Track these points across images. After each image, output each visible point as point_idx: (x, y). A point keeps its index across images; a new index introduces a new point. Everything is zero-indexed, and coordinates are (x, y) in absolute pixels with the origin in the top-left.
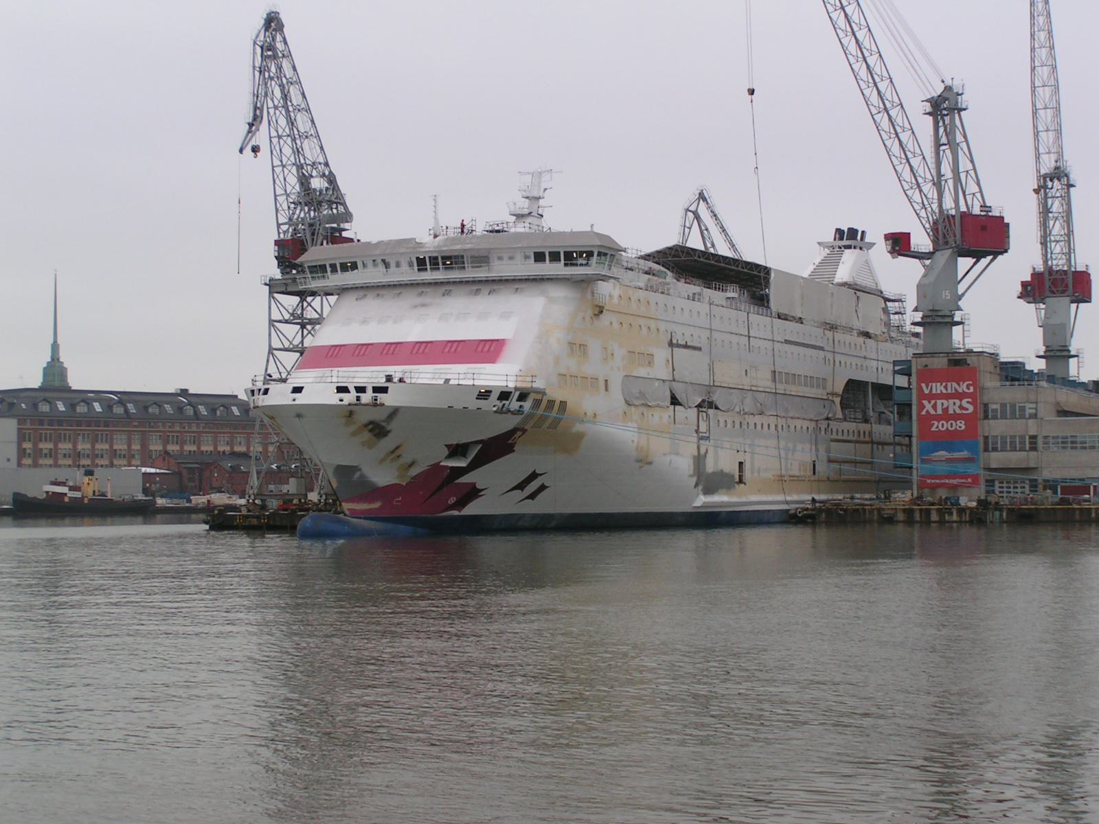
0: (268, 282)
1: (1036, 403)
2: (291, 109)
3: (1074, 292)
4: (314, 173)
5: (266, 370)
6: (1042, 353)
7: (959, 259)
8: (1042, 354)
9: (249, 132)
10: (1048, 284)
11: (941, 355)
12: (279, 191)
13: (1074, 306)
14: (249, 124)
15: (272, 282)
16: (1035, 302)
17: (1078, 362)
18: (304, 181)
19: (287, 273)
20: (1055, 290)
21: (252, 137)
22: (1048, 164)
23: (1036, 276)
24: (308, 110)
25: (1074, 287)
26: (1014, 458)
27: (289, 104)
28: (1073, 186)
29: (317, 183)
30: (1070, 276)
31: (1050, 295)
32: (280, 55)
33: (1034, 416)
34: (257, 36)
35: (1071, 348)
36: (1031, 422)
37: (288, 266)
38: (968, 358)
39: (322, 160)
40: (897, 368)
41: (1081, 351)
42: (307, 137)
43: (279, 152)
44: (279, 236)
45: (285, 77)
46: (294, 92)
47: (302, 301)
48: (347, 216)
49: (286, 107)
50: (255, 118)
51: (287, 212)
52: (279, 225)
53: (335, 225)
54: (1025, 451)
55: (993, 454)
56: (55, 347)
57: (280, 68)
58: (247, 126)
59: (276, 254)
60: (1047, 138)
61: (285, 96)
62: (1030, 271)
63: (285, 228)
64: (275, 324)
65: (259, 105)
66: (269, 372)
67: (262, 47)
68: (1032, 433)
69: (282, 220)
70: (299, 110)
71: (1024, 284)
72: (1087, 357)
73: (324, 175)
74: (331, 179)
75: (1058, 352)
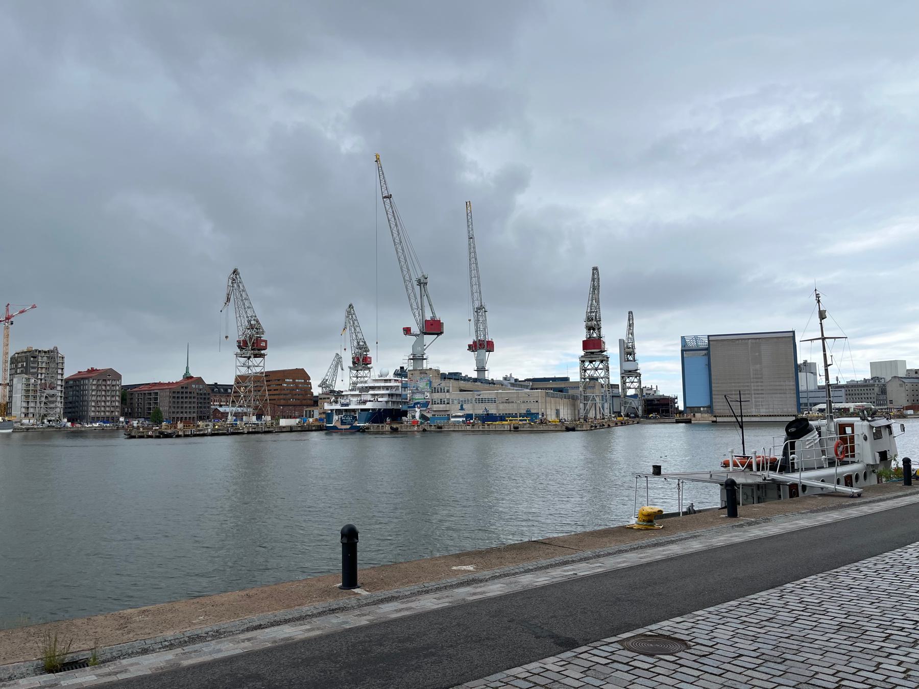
6: (476, 369)
7: (425, 336)
10: (478, 345)
13: (487, 353)
16: (473, 351)
18: (358, 343)
22: (477, 304)
23: (475, 342)
29: (253, 322)
30: (486, 342)
33: (448, 391)
46: (356, 322)
48: (368, 351)
49: (353, 326)
52: (239, 336)
53: (259, 336)
55: (434, 405)
56: (187, 368)
57: (352, 317)
61: (354, 323)
62: (473, 341)
63: (240, 336)
71: (469, 346)
72: (430, 359)
74: (365, 343)
75: (481, 369)
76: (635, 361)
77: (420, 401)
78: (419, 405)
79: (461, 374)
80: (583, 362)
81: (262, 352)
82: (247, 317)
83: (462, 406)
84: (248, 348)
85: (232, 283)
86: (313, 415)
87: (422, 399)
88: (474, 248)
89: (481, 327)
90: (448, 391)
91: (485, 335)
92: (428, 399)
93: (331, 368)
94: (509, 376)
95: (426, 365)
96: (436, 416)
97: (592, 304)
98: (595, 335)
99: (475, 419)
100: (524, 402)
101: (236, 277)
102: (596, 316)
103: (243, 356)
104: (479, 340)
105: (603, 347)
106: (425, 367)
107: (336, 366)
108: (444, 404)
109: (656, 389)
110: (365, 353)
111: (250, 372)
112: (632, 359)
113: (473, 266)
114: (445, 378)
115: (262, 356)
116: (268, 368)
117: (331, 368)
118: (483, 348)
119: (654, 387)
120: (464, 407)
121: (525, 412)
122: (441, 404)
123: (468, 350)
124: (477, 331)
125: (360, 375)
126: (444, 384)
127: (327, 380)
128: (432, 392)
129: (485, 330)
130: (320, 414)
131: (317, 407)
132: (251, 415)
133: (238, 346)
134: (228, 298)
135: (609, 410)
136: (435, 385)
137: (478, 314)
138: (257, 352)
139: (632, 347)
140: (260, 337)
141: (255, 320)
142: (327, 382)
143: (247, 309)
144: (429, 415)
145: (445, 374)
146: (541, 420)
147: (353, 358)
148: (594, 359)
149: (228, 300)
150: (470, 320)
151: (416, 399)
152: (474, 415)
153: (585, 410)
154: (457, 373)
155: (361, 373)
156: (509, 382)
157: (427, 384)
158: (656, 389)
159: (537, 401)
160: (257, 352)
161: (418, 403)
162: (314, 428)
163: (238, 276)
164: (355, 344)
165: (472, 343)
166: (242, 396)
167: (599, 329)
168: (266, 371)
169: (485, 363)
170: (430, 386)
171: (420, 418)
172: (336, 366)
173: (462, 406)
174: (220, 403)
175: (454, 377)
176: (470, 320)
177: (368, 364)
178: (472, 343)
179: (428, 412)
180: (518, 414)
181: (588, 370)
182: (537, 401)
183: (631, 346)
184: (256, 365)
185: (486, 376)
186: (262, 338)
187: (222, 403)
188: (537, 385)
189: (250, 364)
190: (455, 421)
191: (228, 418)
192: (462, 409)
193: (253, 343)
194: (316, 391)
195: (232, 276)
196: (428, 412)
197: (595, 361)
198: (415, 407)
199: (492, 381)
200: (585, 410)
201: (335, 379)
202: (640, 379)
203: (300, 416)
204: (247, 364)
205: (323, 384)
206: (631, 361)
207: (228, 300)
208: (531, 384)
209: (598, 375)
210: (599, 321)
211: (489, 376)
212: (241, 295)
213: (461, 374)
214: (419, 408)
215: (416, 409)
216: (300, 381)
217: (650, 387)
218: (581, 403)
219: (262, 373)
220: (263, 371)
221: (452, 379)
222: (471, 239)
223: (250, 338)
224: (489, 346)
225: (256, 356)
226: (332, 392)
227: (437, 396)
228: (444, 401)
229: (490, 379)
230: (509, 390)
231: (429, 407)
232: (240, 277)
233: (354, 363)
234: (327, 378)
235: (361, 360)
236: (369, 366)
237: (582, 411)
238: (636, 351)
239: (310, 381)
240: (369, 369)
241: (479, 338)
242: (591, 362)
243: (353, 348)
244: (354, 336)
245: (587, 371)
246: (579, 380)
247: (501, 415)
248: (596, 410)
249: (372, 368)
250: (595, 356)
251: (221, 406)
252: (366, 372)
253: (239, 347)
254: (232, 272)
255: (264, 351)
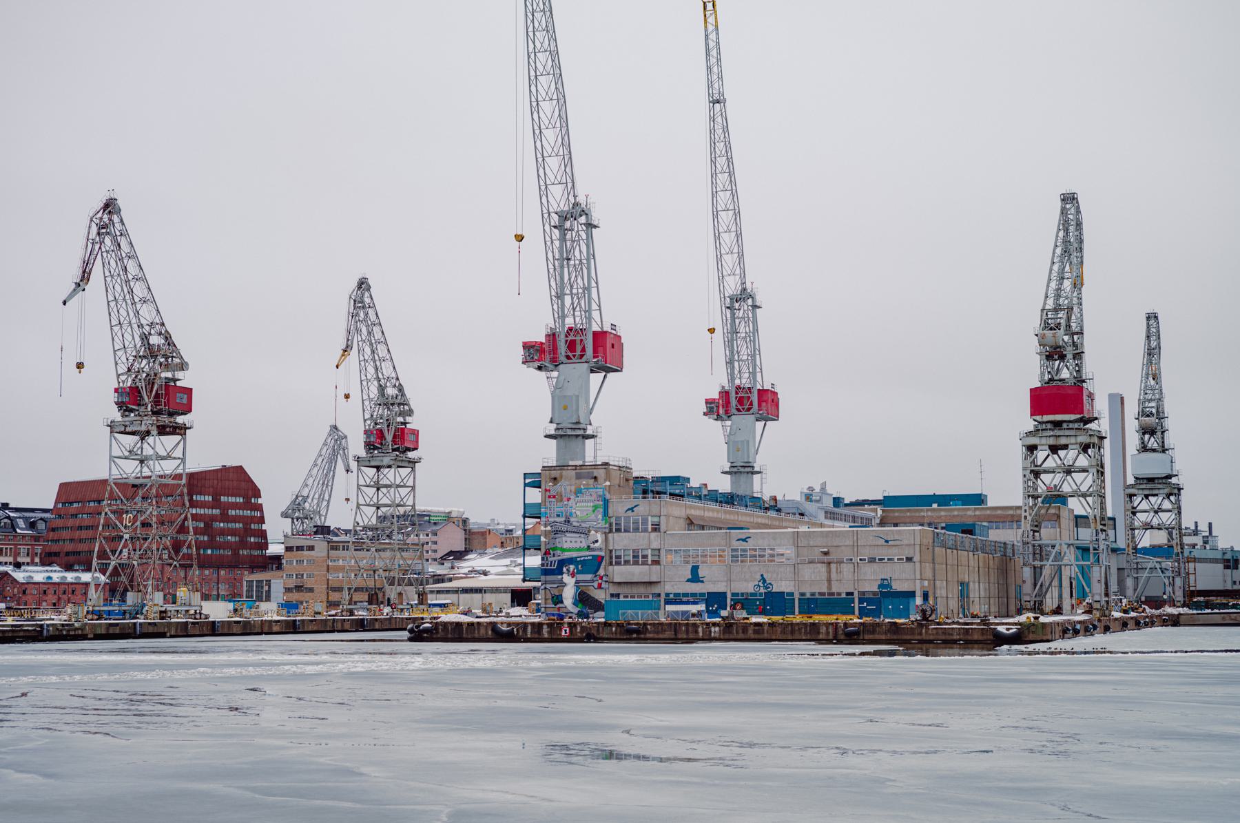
0: (109, 424)
1: (660, 517)
2: (373, 341)
3: (759, 410)
4: (153, 332)
5: (355, 519)
8: (728, 470)
9: (343, 355)
10: (734, 402)
11: (570, 468)
12: (365, 397)
13: (760, 425)
14: (76, 283)
15: (113, 424)
16: (719, 418)
17: (762, 478)
18: (382, 389)
19: (126, 416)
20: (740, 407)
21: (344, 359)
22: (732, 286)
23: (725, 394)
24: (386, 343)
25: (759, 405)
26: (637, 573)
27: (372, 338)
28: (759, 307)
29: (155, 340)
31: (736, 412)
32: (367, 306)
33: (656, 528)
34: (352, 293)
35: (755, 465)
36: (653, 535)
37: (125, 411)
38: (595, 470)
39: (394, 375)
40: (527, 481)
41: (599, 430)
42: (144, 301)
43: (116, 313)
44: (119, 385)
45: (370, 320)
47: (142, 439)
48: (410, 413)
50: (347, 347)
51: (126, 364)
52: (118, 376)
54: (648, 565)
55: (616, 568)
58: (74, 286)
59: (116, 400)
60: (730, 260)
62: (718, 389)
63: (123, 378)
64: (115, 459)
65: (350, 338)
66: (357, 520)
67: (355, 301)
68: (655, 545)
69: (367, 416)
70: (137, 279)
72: (603, 438)
73: (395, 386)
74: (401, 389)
75: (742, 469)
76: (1164, 451)
77: (574, 554)
78: (572, 567)
79: (688, 480)
80: (1032, 449)
81: (180, 419)
82: (140, 326)
83: (695, 569)
84: (142, 409)
85: (99, 234)
86: (269, 592)
87: (580, 549)
88: (726, 129)
89: (744, 351)
90: (656, 528)
91: (753, 374)
92: (600, 549)
93: (316, 465)
94: (817, 489)
95: (591, 453)
96: (622, 598)
97: (1058, 289)
98: (1065, 374)
99: (733, 607)
100: (872, 560)
101: (110, 220)
102: (1069, 319)
103: (128, 429)
104: (738, 388)
105: (1086, 407)
106: (589, 459)
107: (332, 460)
108: (644, 563)
109: (1207, 534)
110: (400, 419)
111: (146, 472)
112: (1155, 446)
113: (723, 178)
114: (645, 492)
115: (180, 430)
116: (193, 466)
117: (316, 465)
118: (749, 410)
119: (1203, 527)
120: (701, 573)
121: (876, 589)
122: (636, 563)
123: (705, 414)
124: (730, 363)
125: (385, 482)
126: (646, 507)
127: (305, 499)
128: (611, 531)
129: (754, 360)
130: (288, 590)
131: (279, 573)
132: (150, 589)
133: (117, 403)
134: (84, 272)
135: (1104, 586)
136: (619, 508)
137: (733, 315)
138: (164, 419)
139: (1158, 412)
140: (175, 380)
141: (160, 334)
142: (307, 505)
143: (138, 306)
144: (600, 596)
145: (646, 480)
146: (924, 612)
147: (366, 432)
148: (1063, 441)
149: (85, 276)
150: (712, 331)
151: (563, 550)
152: (729, 596)
153: (1035, 585)
154: (677, 478)
155: (390, 475)
156: (820, 505)
157: (595, 507)
158: (1207, 534)
159: (909, 559)
160: (164, 419)
161: (571, 561)
162: (275, 629)
163: (115, 218)
164: (374, 391)
165: (717, 397)
166: (127, 536)
167: (1078, 356)
168: (187, 471)
169: (752, 451)
170: (606, 514)
171: (575, 604)
172: (332, 460)
173: (695, 569)
174: (15, 559)
175: (669, 489)
176: (712, 331)
177: (409, 449)
178: (717, 397)
179: (600, 586)
180: (856, 595)
181: (1045, 472)
182: (909, 559)
183: (1154, 411)
184: (164, 454)
185: (756, 487)
186: (178, 384)
187: (20, 560)
188: (897, 512)
189: (148, 451)
190: (677, 613)
191: (90, 596)
192: (695, 578)
193: (157, 395)
194: (277, 531)
195: (100, 215)
196: (600, 586)
197: (1065, 447)
198: (562, 573)
199: (772, 503)
200: (1035, 585)
201: (327, 497)
202: (1179, 501)
203: (232, 597)
204: (139, 452)
205: (296, 511)
206: (1154, 450)
207: (85, 276)
208: (880, 512)
209: (1075, 487)
210: (1077, 333)
211: (764, 487)
212: (125, 269)
213: (688, 480)
214: (573, 575)
215: (566, 578)
216: (231, 499)
217: (1193, 527)
218: (1025, 565)
219: (178, 477)
220: (180, 471)
221: (665, 493)
222: (717, 106)
223: (150, 383)
224: (764, 404)
225: (162, 430)
226: (323, 530)
227: (621, 542)
228: (645, 557)
229: (766, 497)
230: (822, 525)
231: (601, 572)
232: (122, 221)
233: (369, 446)
234: (305, 493)
235: (389, 438)
236: (411, 455)
237: (1027, 588)
238: (1168, 423)
239: (260, 501)
240: (412, 463)
241: (737, 382)
242: (1054, 449)
243: (367, 403)
244: (371, 370)
245: (1043, 476)
246: (1020, 503)
247: (808, 596)
248: (1061, 586)
249: (420, 459)
250: (1067, 432)
251: (18, 565)
252: (404, 472)
253: (120, 405)
254: (102, 205)
255: (183, 417)
